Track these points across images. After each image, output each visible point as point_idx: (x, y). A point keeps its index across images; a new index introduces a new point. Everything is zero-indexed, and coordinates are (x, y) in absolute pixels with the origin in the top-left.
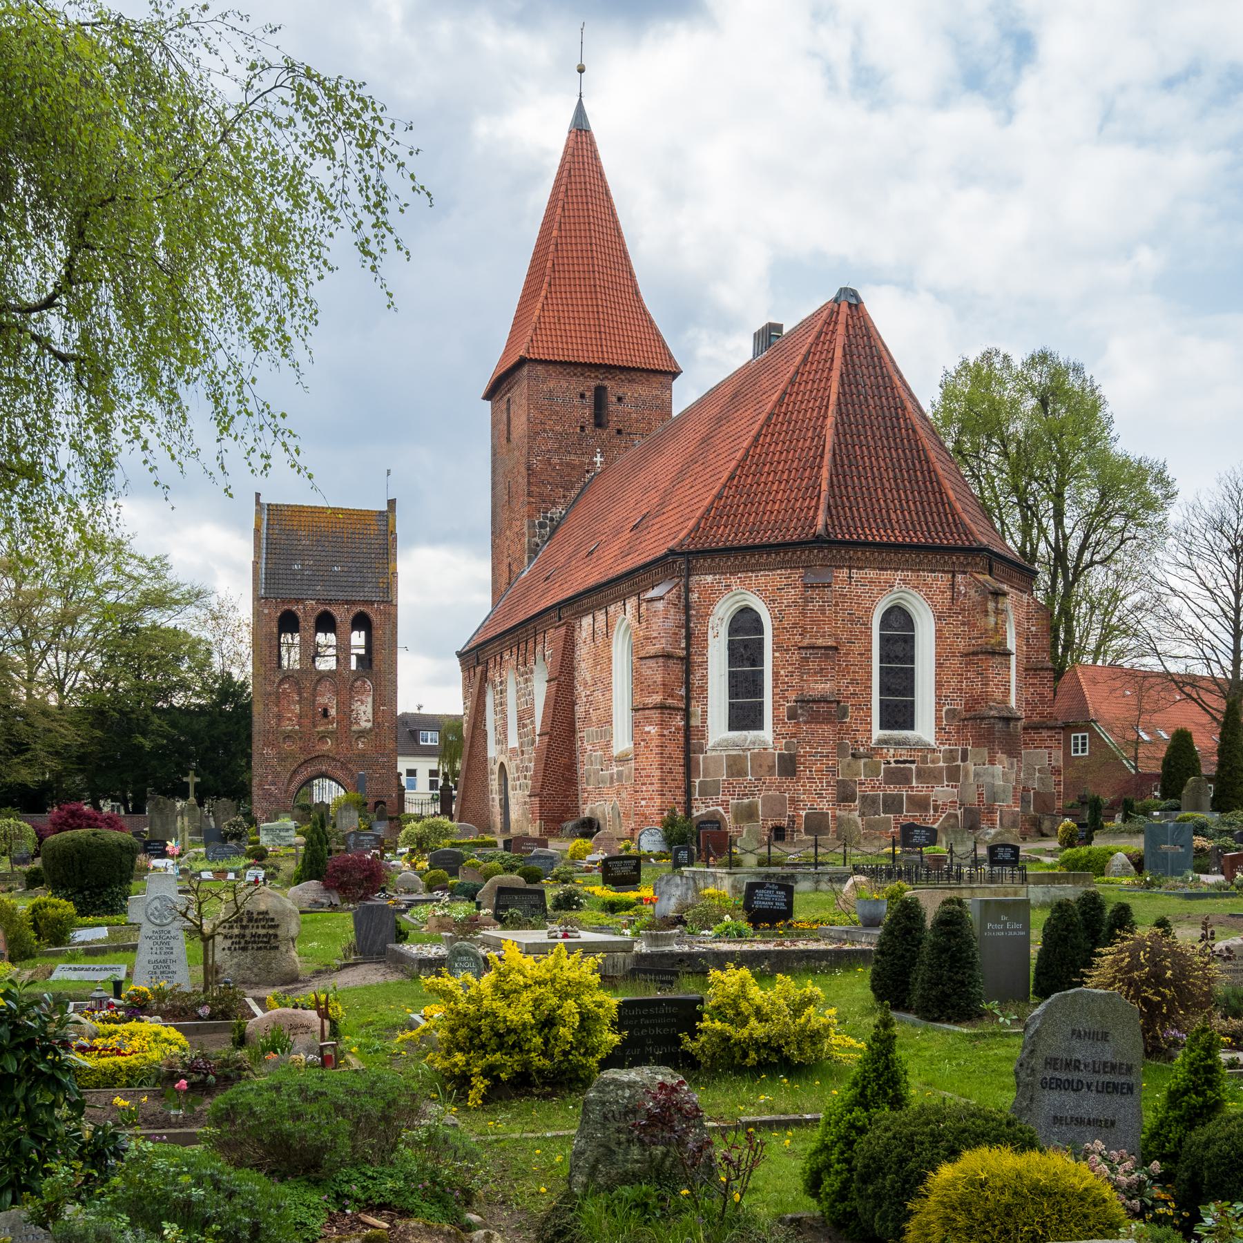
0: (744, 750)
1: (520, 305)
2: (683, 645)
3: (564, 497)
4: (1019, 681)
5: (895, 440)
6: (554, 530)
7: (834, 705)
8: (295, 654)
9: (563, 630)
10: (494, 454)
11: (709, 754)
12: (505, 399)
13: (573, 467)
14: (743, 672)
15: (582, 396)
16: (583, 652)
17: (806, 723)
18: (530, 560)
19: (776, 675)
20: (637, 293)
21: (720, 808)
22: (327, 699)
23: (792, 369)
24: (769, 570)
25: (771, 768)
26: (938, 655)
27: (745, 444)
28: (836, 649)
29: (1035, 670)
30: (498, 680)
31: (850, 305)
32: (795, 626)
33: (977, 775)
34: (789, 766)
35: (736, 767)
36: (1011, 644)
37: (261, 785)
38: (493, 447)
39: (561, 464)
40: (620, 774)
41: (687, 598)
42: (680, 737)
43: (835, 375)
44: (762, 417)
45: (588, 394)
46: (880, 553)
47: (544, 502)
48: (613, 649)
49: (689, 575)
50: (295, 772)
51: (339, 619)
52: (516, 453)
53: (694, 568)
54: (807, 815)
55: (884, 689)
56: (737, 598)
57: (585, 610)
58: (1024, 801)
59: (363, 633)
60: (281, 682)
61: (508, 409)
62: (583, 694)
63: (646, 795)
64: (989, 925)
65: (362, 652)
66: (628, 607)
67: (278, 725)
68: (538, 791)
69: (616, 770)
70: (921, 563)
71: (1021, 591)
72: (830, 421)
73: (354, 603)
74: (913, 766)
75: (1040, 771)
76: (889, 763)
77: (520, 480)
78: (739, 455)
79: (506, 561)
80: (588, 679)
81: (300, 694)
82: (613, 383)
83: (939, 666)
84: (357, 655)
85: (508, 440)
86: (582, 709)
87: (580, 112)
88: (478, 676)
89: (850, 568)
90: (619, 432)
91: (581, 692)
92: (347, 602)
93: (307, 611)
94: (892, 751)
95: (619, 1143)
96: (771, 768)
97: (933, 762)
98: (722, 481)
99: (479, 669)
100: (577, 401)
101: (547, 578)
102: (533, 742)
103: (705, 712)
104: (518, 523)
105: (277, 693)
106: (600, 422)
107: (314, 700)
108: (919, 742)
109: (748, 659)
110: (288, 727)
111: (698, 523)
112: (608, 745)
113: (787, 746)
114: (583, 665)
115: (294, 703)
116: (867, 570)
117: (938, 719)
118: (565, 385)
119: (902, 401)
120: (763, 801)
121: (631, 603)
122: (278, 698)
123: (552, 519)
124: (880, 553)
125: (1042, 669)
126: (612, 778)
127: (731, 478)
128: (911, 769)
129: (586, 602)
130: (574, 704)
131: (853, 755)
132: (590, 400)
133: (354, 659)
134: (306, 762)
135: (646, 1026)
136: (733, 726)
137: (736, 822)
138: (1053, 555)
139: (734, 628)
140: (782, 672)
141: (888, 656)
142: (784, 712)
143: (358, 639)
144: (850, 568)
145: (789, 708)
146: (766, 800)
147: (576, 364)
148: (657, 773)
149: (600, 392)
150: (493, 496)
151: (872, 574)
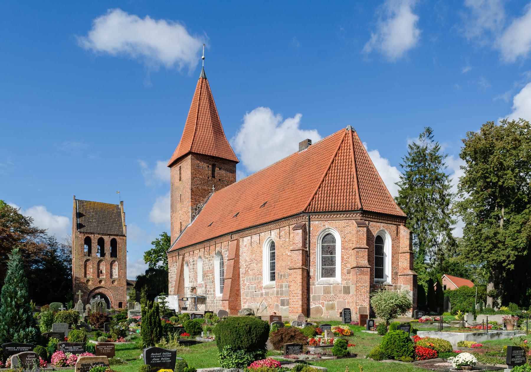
3: (203, 200)
17: (359, 275)
21: (321, 305)
25: (340, 291)
35: (327, 291)
39: (202, 189)
47: (196, 201)
54: (359, 308)
83: (393, 256)
90: (220, 180)
92: (109, 235)
96: (340, 291)
101: (210, 225)
109: (329, 252)
112: (260, 282)
137: (327, 310)
140: (345, 257)
142: (345, 271)
146: (338, 302)
148: (301, 292)
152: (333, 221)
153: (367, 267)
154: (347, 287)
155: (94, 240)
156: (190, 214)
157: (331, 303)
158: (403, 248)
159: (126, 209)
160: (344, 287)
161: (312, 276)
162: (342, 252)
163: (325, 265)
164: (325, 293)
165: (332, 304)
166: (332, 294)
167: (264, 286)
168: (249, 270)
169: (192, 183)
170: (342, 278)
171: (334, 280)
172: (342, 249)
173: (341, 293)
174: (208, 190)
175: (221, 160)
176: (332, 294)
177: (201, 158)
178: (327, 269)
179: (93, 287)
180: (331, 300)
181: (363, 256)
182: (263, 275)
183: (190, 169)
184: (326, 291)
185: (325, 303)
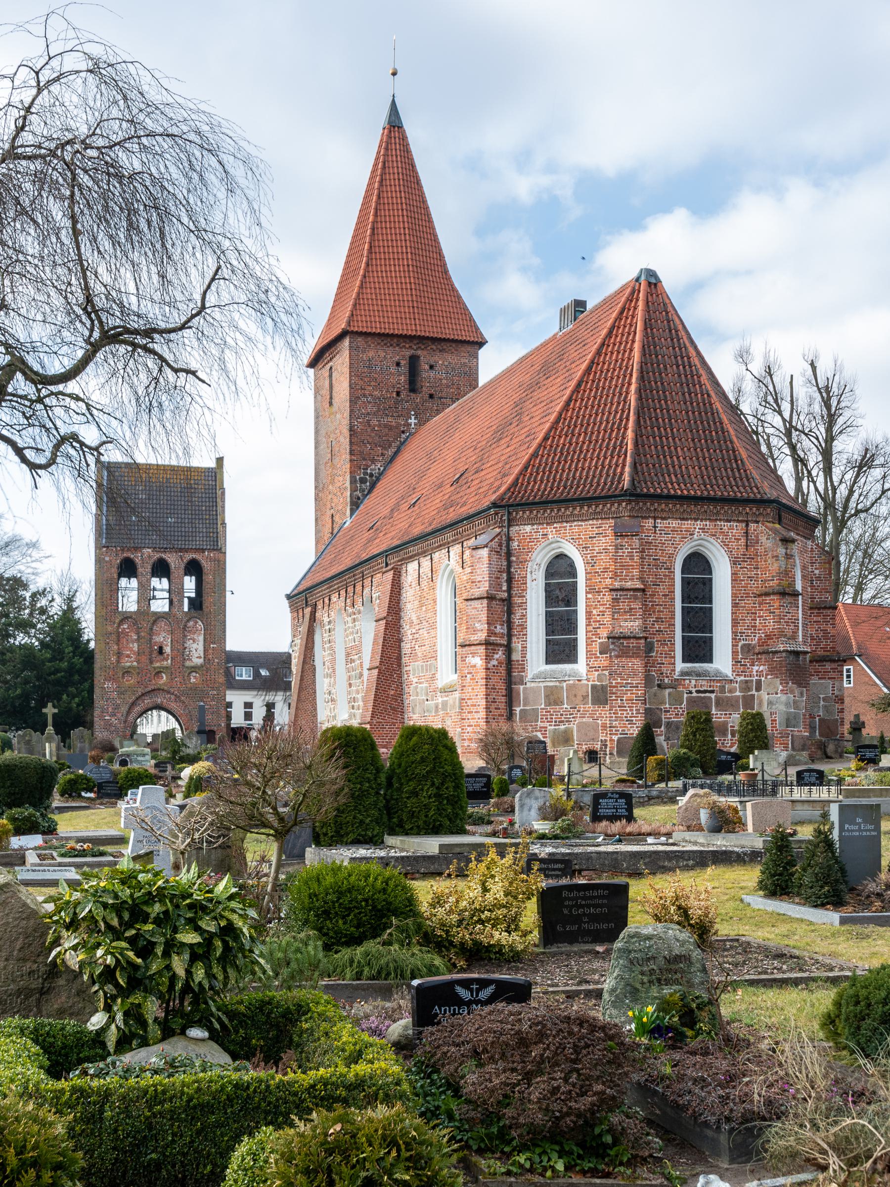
0: (560, 682)
1: (340, 283)
2: (505, 588)
3: (383, 455)
4: (804, 619)
5: (692, 404)
6: (373, 486)
7: (643, 641)
8: (134, 595)
9: (390, 575)
10: (317, 417)
11: (528, 685)
12: (328, 367)
13: (391, 428)
14: (558, 612)
15: (398, 364)
16: (409, 594)
17: (617, 657)
18: (352, 512)
19: (589, 614)
20: (446, 272)
22: (163, 638)
23: (599, 341)
24: (582, 521)
26: (734, 596)
27: (558, 408)
28: (643, 590)
29: (819, 609)
30: (326, 620)
31: (650, 284)
32: (605, 570)
33: (770, 703)
34: (600, 696)
35: (553, 697)
36: (799, 587)
37: (102, 717)
38: (316, 410)
39: (379, 426)
40: (445, 704)
41: (508, 546)
42: (503, 670)
43: (637, 346)
44: (573, 383)
45: (403, 363)
46: (682, 505)
47: (364, 459)
48: (438, 592)
49: (509, 526)
50: (133, 704)
51: (173, 566)
52: (338, 416)
53: (514, 519)
55: (686, 627)
56: (553, 545)
57: (411, 557)
58: (812, 728)
59: (193, 578)
60: (121, 622)
61: (331, 376)
62: (409, 632)
63: (472, 722)
64: (847, 826)
65: (193, 595)
66: (451, 554)
67: (118, 662)
68: (369, 719)
69: (440, 700)
70: (718, 513)
71: (805, 538)
72: (633, 388)
73: (187, 550)
74: (713, 696)
75: (824, 699)
76: (691, 692)
77: (342, 439)
78: (553, 417)
79: (329, 513)
80: (414, 618)
81: (138, 634)
82: (425, 352)
83: (735, 605)
84: (189, 598)
85: (331, 404)
86: (408, 646)
87: (393, 103)
88: (307, 616)
89: (655, 518)
90: (431, 396)
91: (408, 631)
93: (145, 557)
94: (693, 682)
95: (643, 983)
96: (585, 697)
97: (730, 691)
98: (538, 441)
99: (308, 610)
100: (393, 369)
101: (372, 528)
102: (361, 675)
103: (524, 648)
104: (341, 479)
105: (119, 632)
106: (413, 386)
107: (151, 639)
108: (718, 673)
110: (127, 663)
111: (517, 479)
112: (433, 678)
113: (600, 678)
114: (409, 606)
115: (133, 642)
116: (670, 521)
117: (735, 653)
118: (383, 354)
119: (697, 370)
120: (578, 727)
121: (456, 550)
122: (119, 637)
123: (371, 475)
124: (682, 505)
125: (825, 608)
126: (437, 707)
127: (546, 438)
128: (710, 698)
129: (413, 550)
130: (400, 641)
131: (659, 686)
132: (404, 368)
133: (186, 601)
134: (143, 695)
135: (582, 906)
136: (548, 661)
138: (822, 505)
139: (550, 573)
140: (594, 612)
141: (689, 597)
142: (596, 647)
143: (189, 583)
144: (655, 518)
145: (601, 643)
147: (393, 336)
148: (483, 703)
149: (414, 361)
150: (317, 454)
151: (674, 524)
152: (565, 524)
153: (635, 638)
154: (600, 688)
155: (142, 567)
156: (349, 493)
157: (562, 727)
158: (766, 581)
159: (230, 480)
160: (594, 687)
161: (518, 661)
162: (587, 599)
163: (553, 632)
164: (550, 704)
165: (566, 731)
166: (565, 706)
167: (440, 687)
168: (417, 647)
169: (351, 411)
170: (588, 665)
171: (573, 669)
172: (587, 593)
173: (587, 703)
174: (397, 427)
175: (433, 344)
176: (565, 706)
177: (379, 344)
178: (557, 643)
179: (140, 690)
180: (563, 722)
181: (631, 609)
182: (439, 658)
183: (348, 375)
184: (552, 697)
185: (549, 728)
